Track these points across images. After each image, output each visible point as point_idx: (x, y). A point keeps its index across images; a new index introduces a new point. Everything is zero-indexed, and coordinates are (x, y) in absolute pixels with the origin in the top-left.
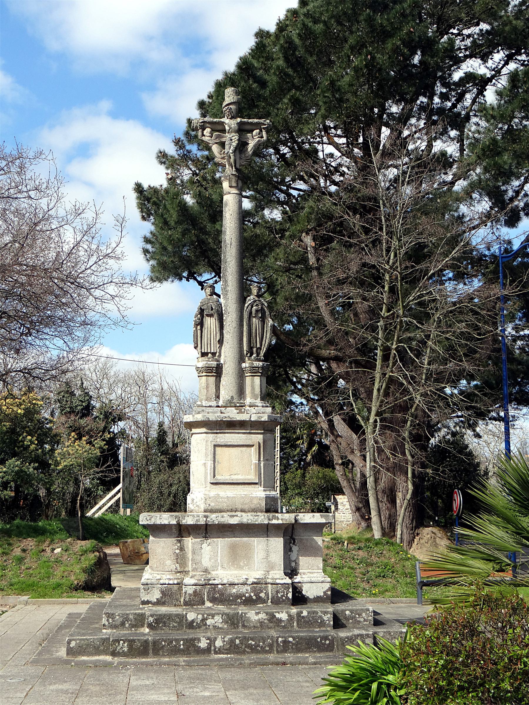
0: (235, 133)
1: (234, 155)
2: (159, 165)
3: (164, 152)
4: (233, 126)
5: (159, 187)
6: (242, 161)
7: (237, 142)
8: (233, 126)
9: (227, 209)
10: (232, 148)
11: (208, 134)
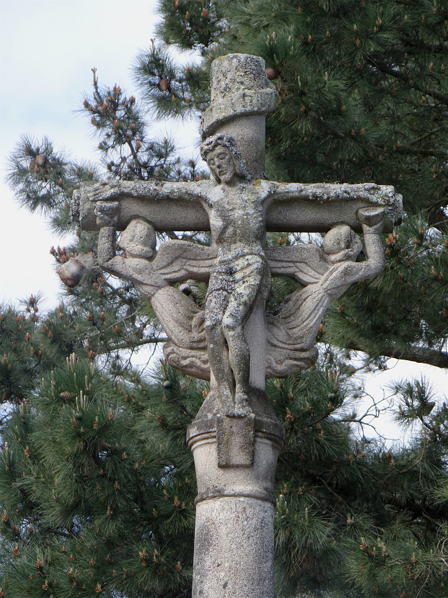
0: (248, 242)
1: (243, 338)
2: (25, 210)
3: (48, 150)
4: (238, 214)
5: (20, 308)
6: (278, 354)
7: (254, 281)
8: (238, 214)
9: (208, 562)
10: (233, 304)
11: (137, 248)
